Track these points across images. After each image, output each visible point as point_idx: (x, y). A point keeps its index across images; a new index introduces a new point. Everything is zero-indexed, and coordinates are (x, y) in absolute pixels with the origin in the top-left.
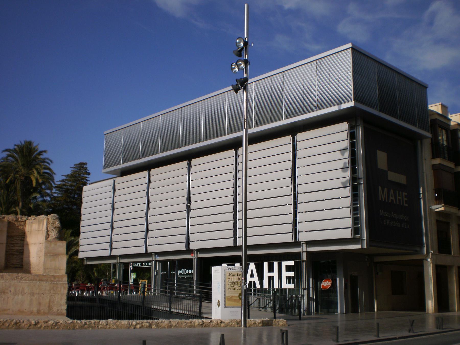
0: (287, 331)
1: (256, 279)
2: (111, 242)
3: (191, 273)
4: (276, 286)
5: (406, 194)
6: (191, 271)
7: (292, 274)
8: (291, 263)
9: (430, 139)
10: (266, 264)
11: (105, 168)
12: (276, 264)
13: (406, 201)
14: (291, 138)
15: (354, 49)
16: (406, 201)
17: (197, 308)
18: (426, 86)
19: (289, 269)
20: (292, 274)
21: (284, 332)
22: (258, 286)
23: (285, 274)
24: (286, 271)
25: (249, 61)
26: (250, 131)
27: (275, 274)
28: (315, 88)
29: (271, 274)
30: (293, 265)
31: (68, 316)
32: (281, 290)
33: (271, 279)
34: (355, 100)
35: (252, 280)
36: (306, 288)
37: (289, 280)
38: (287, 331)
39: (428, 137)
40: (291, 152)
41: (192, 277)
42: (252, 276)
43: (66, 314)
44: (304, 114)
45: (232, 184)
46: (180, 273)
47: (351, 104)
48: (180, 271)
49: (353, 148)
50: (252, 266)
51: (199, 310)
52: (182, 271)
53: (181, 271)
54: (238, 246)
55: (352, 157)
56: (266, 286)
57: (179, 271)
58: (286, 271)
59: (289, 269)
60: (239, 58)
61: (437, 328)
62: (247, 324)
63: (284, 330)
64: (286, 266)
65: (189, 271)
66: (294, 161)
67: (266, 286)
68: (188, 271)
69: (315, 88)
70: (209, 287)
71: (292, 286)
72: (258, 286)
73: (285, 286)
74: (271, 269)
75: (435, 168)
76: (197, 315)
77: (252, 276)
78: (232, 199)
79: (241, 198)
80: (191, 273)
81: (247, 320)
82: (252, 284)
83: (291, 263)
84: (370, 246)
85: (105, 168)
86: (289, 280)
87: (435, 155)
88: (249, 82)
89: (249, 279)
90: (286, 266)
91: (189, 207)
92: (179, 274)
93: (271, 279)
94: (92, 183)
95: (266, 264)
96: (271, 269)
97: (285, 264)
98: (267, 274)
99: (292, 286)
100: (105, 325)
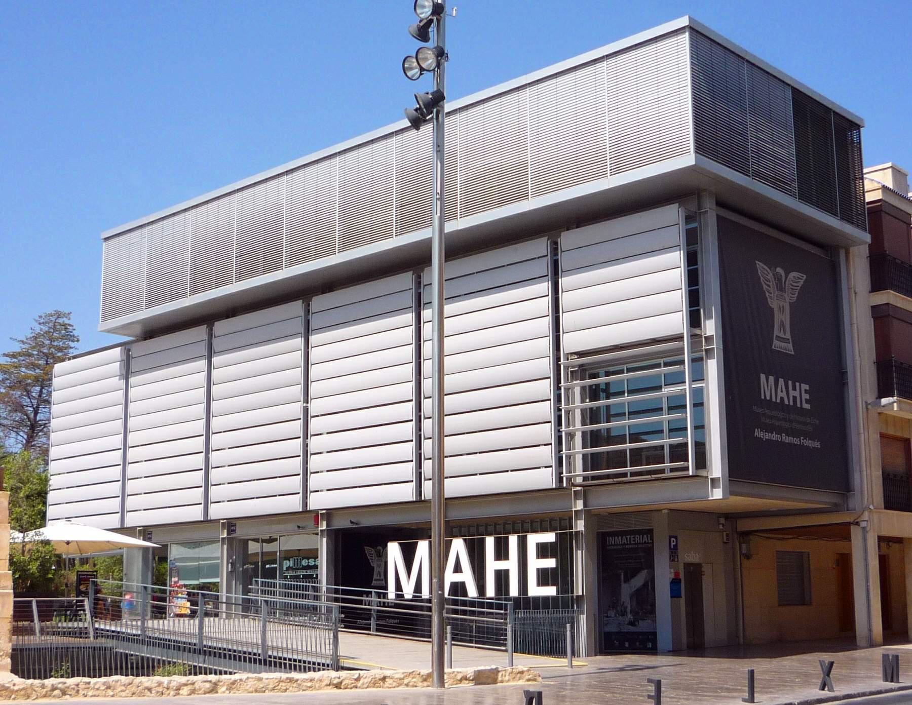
0: (540, 694)
1: (467, 577)
2: (123, 496)
3: (315, 565)
4: (514, 591)
5: (807, 387)
6: (315, 561)
7: (550, 563)
8: (549, 537)
9: (867, 246)
10: (490, 542)
11: (105, 319)
12: (513, 540)
13: (806, 399)
14: (549, 242)
15: (696, 33)
16: (806, 399)
17: (327, 647)
18: (858, 122)
19: (544, 551)
20: (550, 563)
21: (532, 696)
22: (472, 592)
23: (535, 564)
24: (538, 557)
25: (446, 52)
26: (451, 227)
27: (511, 565)
28: (604, 120)
29: (502, 565)
30: (554, 568)
31: (14, 671)
32: (524, 602)
33: (502, 577)
34: (700, 147)
35: (458, 578)
36: (584, 594)
37: (544, 577)
38: (540, 694)
39: (864, 243)
40: (548, 275)
41: (317, 575)
42: (458, 569)
43: (10, 667)
44: (577, 183)
45: (410, 351)
46: (287, 566)
47: (689, 159)
48: (288, 562)
49: (692, 268)
50: (458, 546)
51: (331, 651)
52: (291, 562)
53: (290, 561)
54: (425, 501)
55: (690, 289)
56: (491, 591)
57: (285, 562)
58: (538, 557)
59: (544, 551)
60: (423, 44)
61: (886, 680)
62: (445, 681)
63: (534, 692)
64: (538, 570)
65: (310, 561)
66: (556, 335)
67: (491, 591)
68: (307, 561)
69: (604, 120)
70: (362, 605)
71: (550, 591)
72: (472, 592)
73: (535, 590)
74: (502, 553)
75: (881, 315)
76: (328, 662)
77: (458, 569)
78: (409, 389)
79: (428, 385)
80: (315, 565)
81: (447, 670)
82: (459, 588)
83: (549, 537)
84: (732, 493)
85: (105, 319)
86: (544, 577)
87: (877, 286)
88: (448, 107)
89: (450, 577)
90: (538, 570)
91: (306, 410)
92: (285, 569)
93: (502, 577)
94: (75, 357)
95: (490, 542)
96: (502, 553)
97: (534, 539)
98: (492, 565)
99: (550, 591)
100: (104, 690)
